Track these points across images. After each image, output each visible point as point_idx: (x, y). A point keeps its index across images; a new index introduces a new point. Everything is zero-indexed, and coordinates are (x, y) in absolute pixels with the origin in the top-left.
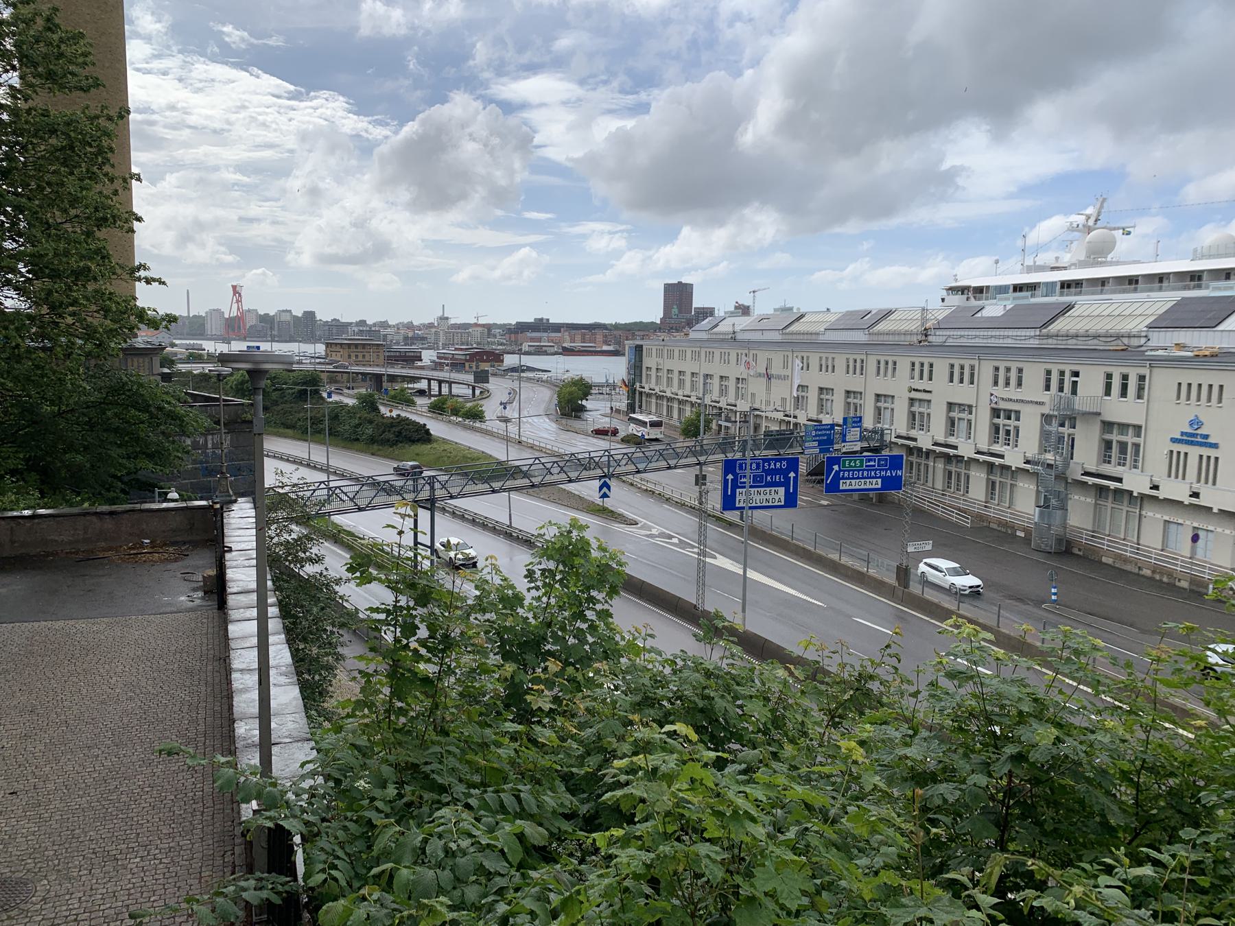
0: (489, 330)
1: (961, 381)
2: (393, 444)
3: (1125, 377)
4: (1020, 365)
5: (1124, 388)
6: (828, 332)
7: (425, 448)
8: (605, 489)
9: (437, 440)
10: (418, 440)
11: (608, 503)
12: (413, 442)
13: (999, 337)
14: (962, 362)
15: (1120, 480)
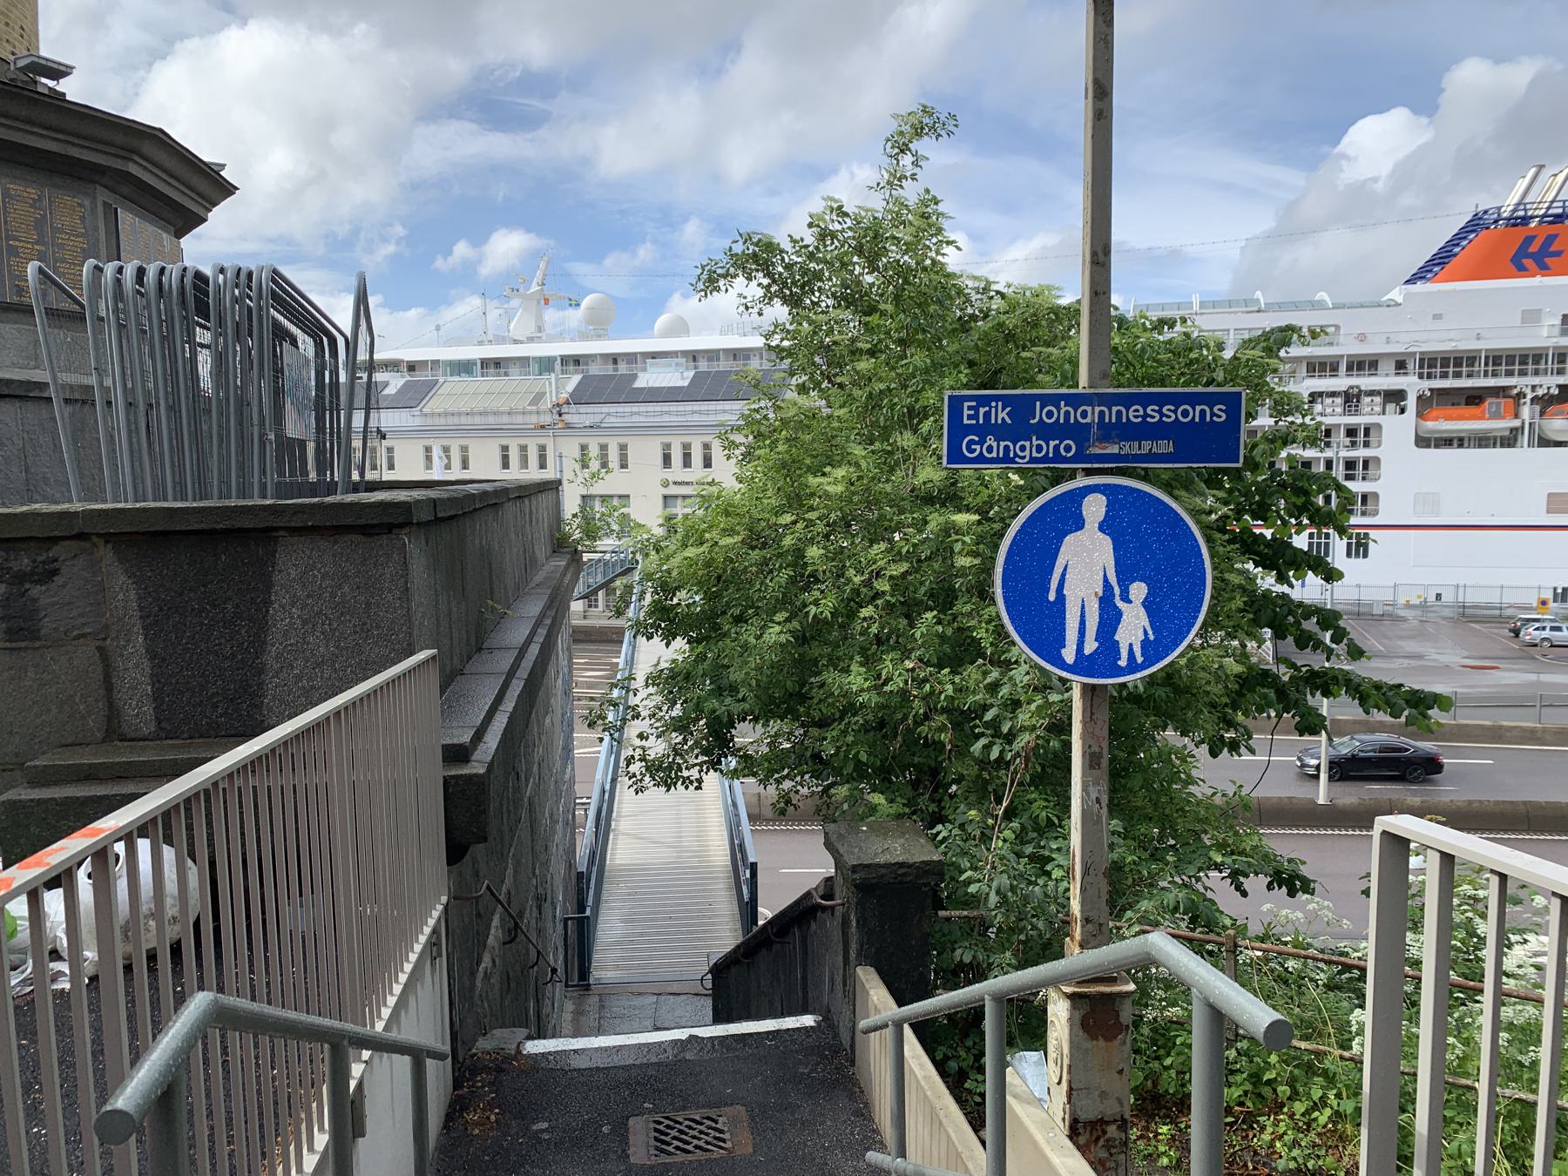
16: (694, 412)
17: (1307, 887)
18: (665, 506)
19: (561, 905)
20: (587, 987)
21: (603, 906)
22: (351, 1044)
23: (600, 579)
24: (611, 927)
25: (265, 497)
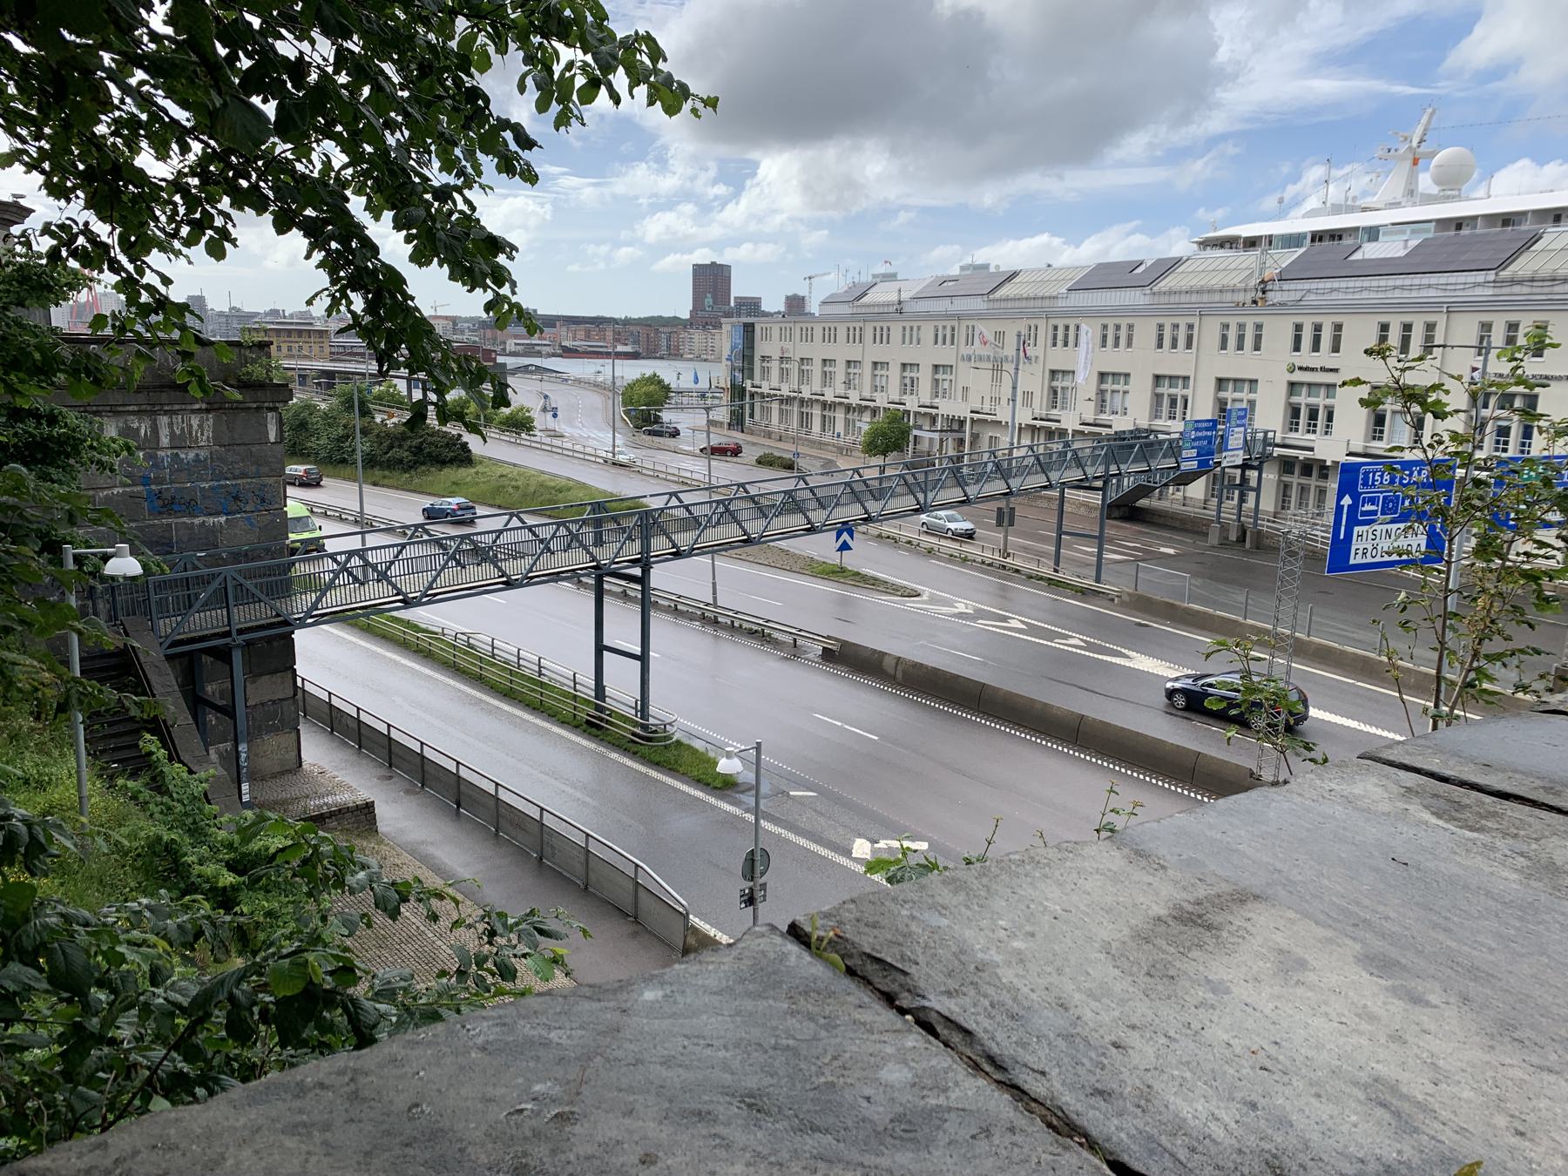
0: (455, 324)
1: (1240, 347)
2: (410, 467)
3: (1318, 328)
4: (1258, 320)
5: (1241, 338)
6: (1073, 295)
7: (464, 473)
8: (845, 536)
9: (482, 460)
10: (451, 461)
11: (850, 560)
12: (443, 463)
13: (1411, 288)
14: (1241, 320)
15: (1311, 449)
17: (759, 462)
22: (190, 1036)
25: (931, 440)
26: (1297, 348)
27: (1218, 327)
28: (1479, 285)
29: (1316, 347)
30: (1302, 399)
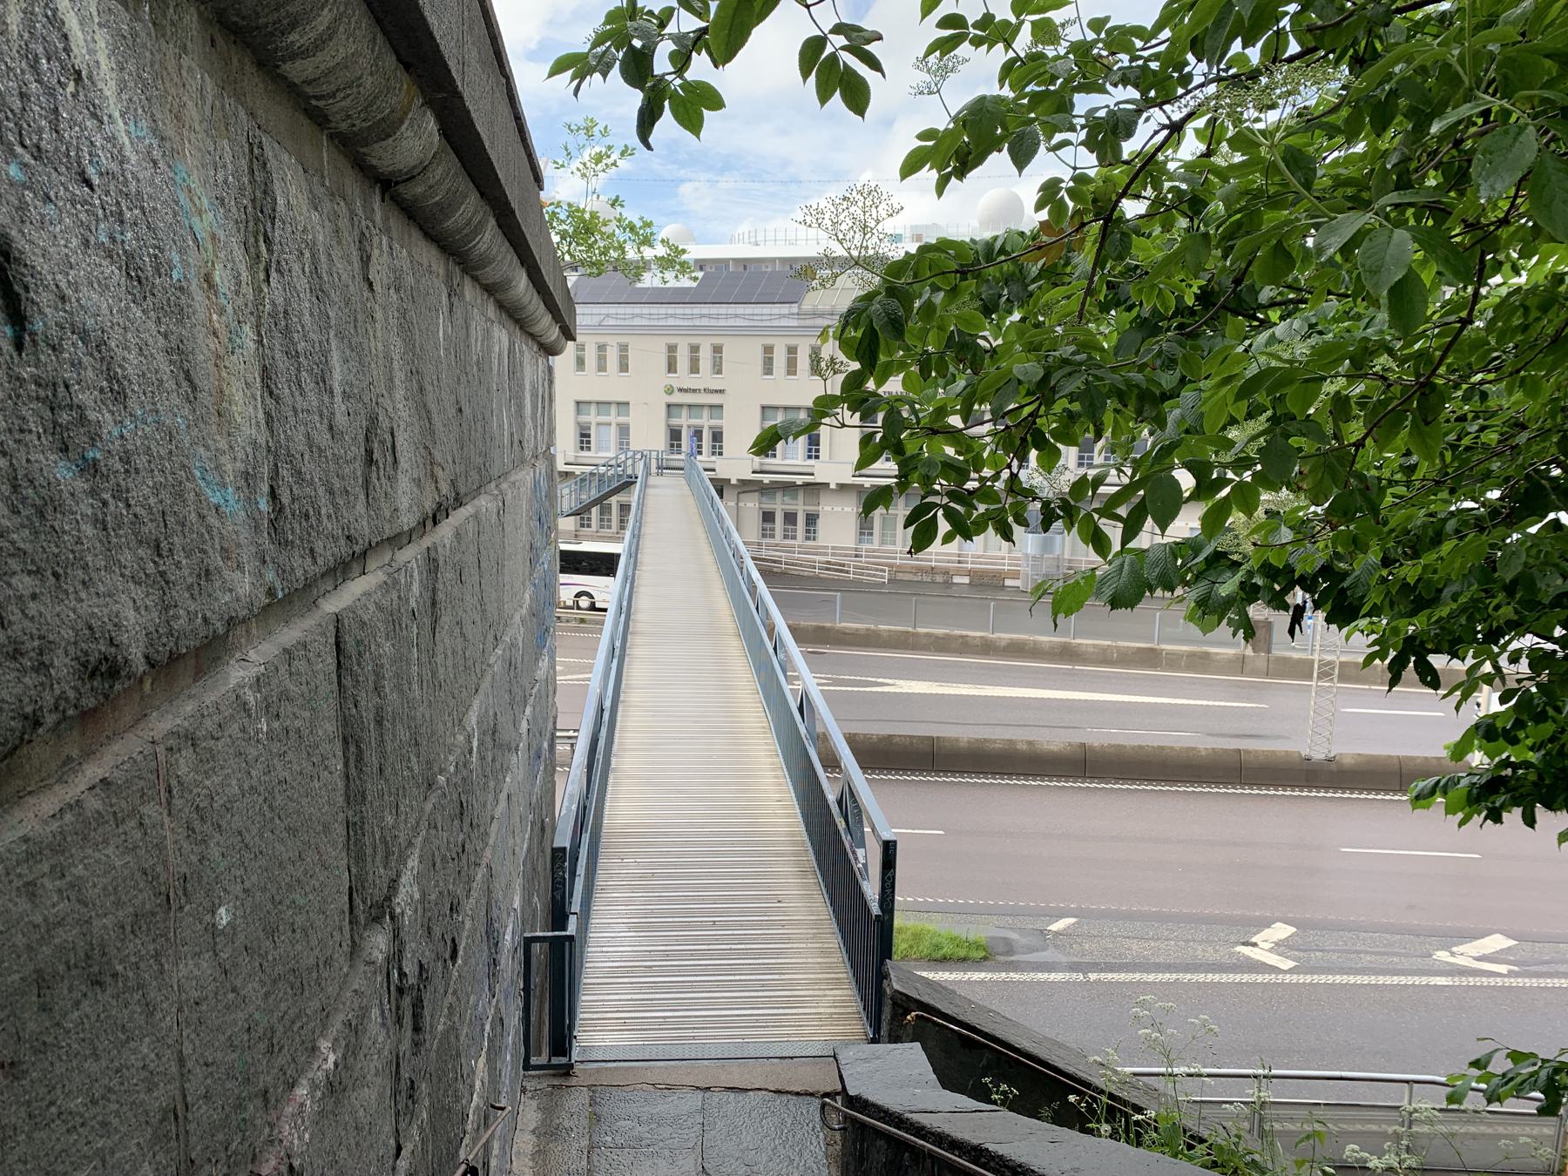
16: (702, 316)
18: (669, 415)
19: (516, 908)
20: (567, 1071)
21: (598, 896)
23: (594, 494)
24: (612, 942)
26: (672, 367)
27: (664, 349)
28: (784, 316)
29: (694, 368)
30: (684, 421)
